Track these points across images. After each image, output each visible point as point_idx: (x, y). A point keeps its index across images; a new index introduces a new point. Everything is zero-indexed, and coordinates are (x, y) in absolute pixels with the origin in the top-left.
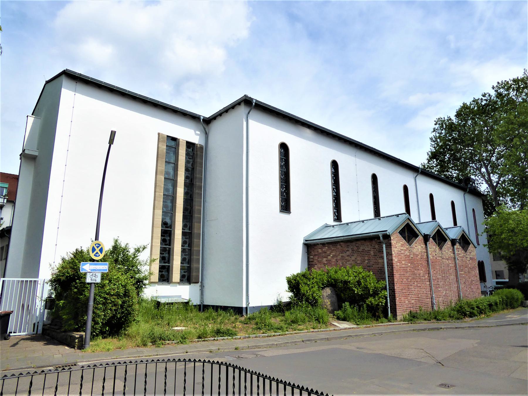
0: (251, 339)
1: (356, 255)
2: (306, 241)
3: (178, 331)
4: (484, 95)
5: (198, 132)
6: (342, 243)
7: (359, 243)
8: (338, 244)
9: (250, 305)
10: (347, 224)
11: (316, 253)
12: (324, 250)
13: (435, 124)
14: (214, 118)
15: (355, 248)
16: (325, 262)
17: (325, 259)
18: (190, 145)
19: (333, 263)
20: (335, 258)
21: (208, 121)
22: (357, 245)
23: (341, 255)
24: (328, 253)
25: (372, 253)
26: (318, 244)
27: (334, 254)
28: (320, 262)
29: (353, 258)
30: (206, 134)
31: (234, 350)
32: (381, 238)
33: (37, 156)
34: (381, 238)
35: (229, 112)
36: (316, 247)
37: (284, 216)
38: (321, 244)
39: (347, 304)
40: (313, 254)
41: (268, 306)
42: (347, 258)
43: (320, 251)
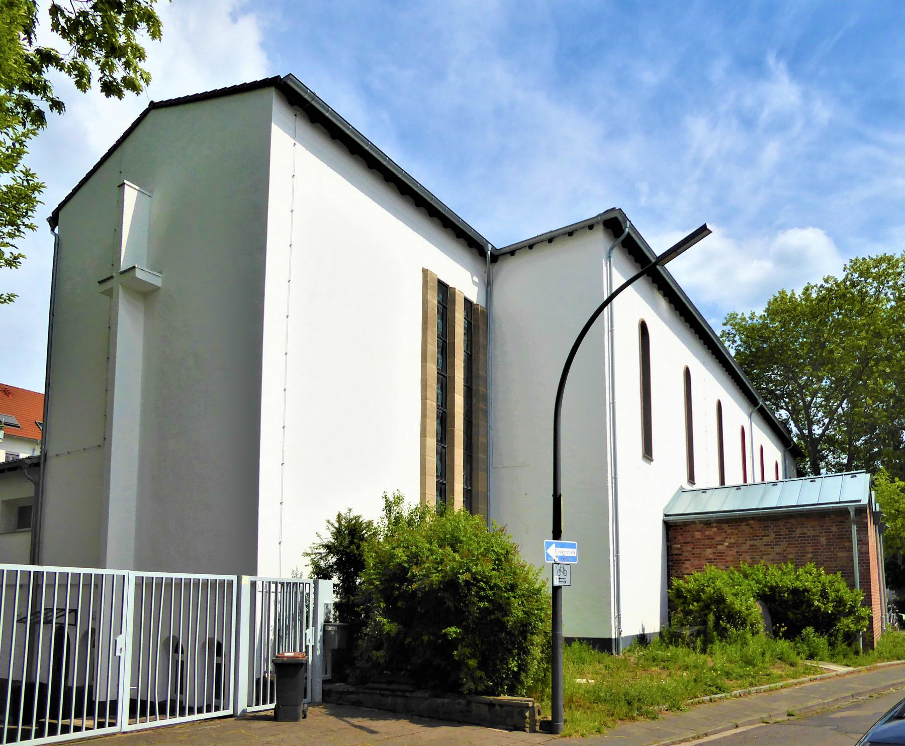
0: (753, 697)
1: (784, 544)
2: (666, 515)
3: (580, 685)
4: (826, 281)
5: (476, 279)
6: (752, 522)
7: (793, 521)
8: (745, 523)
9: (623, 635)
10: (704, 491)
11: (689, 540)
12: (707, 533)
13: (725, 324)
14: (512, 252)
15: (784, 531)
16: (711, 556)
17: (709, 551)
18: (467, 302)
19: (729, 559)
20: (735, 549)
21: (497, 257)
22: (789, 526)
23: (749, 543)
24: (719, 539)
25: (823, 540)
26: (694, 523)
27: (732, 541)
28: (699, 557)
29: (777, 549)
30: (488, 286)
31: (786, 718)
32: (852, 514)
33: (157, 289)
34: (852, 514)
35: (574, 236)
36: (688, 528)
37: (644, 464)
38: (701, 522)
39: (810, 629)
40: (682, 541)
41: (633, 637)
42: (763, 548)
43: (698, 535)
